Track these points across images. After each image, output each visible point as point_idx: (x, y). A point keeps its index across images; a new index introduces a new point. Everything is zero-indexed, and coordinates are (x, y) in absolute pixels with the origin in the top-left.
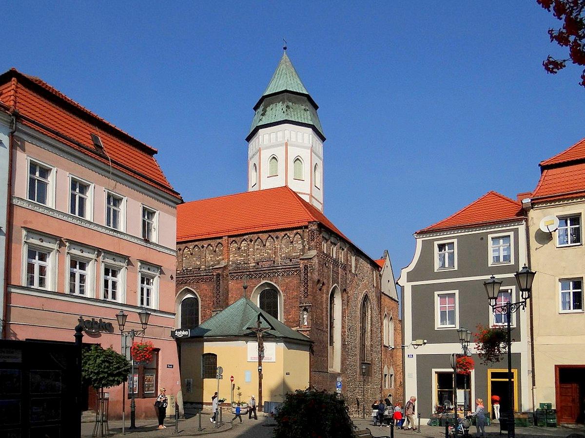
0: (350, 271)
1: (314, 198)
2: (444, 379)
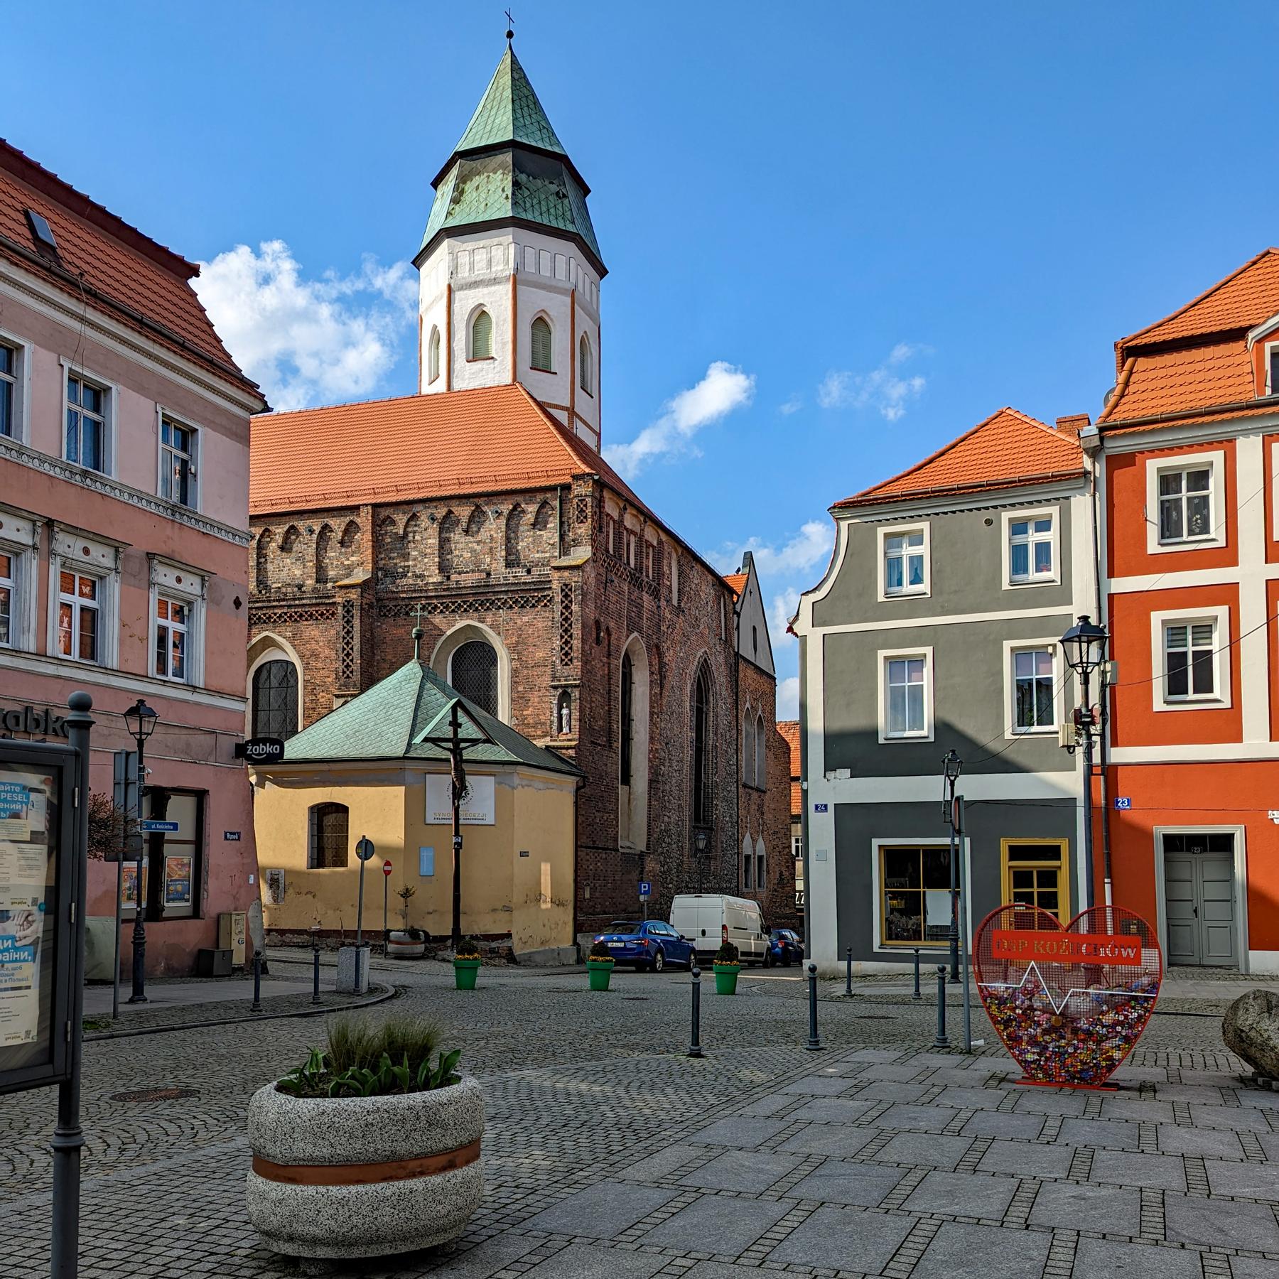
0: (669, 601)
1: (581, 419)
2: (897, 861)
